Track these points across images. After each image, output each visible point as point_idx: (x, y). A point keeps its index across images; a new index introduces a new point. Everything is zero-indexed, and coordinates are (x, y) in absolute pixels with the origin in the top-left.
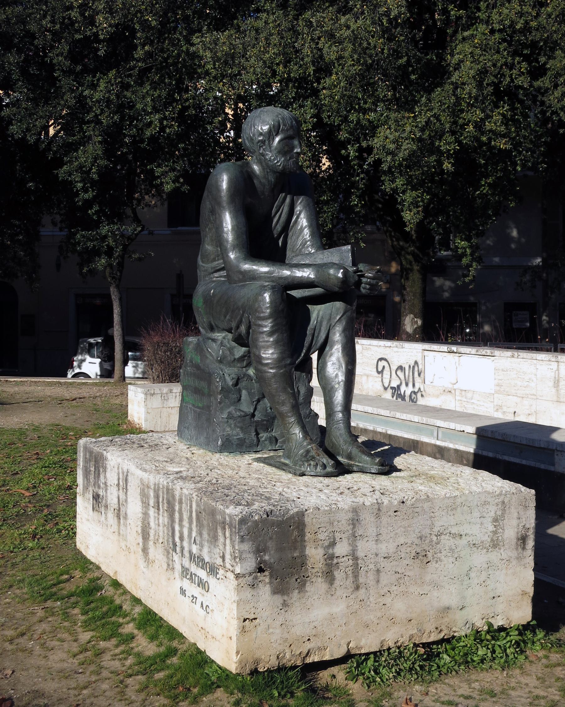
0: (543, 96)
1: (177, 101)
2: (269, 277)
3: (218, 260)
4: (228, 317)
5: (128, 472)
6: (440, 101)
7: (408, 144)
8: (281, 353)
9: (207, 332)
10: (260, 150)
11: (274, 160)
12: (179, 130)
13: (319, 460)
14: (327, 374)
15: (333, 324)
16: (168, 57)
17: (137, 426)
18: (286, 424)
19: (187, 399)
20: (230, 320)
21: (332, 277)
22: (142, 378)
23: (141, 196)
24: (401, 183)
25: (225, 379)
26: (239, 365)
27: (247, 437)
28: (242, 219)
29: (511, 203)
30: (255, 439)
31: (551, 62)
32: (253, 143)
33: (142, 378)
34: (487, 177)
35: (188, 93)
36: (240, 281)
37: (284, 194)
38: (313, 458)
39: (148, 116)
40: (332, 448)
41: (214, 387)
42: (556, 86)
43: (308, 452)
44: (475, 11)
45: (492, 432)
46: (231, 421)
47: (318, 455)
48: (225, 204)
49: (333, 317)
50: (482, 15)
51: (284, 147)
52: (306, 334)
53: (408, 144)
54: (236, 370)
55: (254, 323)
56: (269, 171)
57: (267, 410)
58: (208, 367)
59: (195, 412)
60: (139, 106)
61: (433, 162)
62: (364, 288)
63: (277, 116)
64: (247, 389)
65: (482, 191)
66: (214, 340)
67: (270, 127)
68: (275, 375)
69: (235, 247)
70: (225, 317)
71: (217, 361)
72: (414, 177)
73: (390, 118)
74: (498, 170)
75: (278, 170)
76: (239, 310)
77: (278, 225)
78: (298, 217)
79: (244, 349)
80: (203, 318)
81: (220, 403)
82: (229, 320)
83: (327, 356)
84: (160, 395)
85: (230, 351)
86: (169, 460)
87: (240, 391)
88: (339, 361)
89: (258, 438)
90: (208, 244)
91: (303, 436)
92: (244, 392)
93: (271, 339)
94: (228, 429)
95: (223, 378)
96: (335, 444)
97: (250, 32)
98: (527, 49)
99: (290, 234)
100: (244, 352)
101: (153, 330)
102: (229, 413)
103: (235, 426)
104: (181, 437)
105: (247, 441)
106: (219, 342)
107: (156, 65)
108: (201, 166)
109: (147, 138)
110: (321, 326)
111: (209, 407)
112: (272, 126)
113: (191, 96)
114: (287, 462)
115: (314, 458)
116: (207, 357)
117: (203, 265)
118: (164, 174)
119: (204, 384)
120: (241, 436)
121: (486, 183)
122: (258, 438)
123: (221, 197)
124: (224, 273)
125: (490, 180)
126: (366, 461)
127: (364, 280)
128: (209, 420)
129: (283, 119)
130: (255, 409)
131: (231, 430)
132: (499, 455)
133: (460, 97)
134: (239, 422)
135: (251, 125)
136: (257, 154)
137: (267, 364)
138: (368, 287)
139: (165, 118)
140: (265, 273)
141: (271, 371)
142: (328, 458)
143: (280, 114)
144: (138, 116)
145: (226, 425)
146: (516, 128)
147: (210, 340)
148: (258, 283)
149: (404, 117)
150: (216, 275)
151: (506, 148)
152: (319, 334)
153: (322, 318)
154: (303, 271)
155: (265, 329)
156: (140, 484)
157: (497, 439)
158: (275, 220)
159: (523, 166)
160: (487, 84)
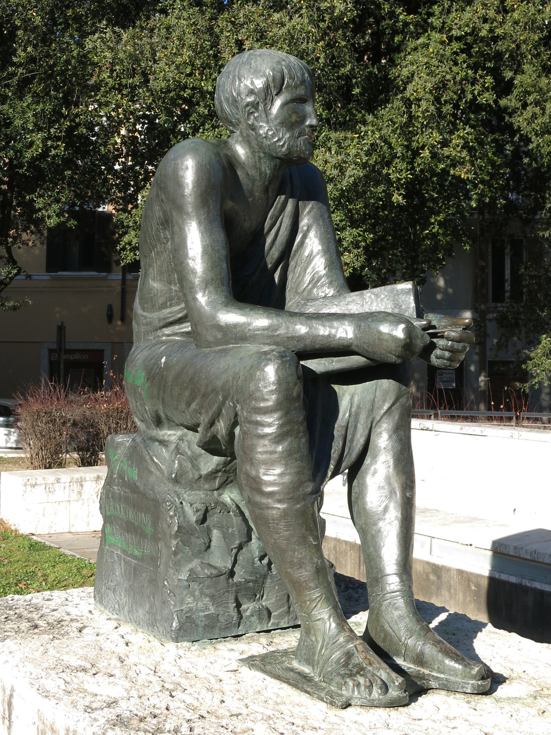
0: (511, 117)
1: (65, 117)
2: (269, 337)
3: (171, 306)
4: (193, 406)
5: (12, 690)
6: (391, 120)
7: (353, 169)
8: (299, 473)
9: (148, 428)
10: (248, 119)
11: (273, 136)
12: (65, 155)
13: (374, 675)
14: (364, 503)
15: (378, 418)
16: (55, 65)
17: (13, 528)
18: (305, 602)
19: (111, 539)
20: (198, 412)
21: (386, 337)
22: (16, 448)
23: (18, 234)
24: (338, 218)
25: (184, 512)
26: (207, 486)
27: (222, 612)
28: (220, 236)
29: (465, 245)
30: (235, 614)
31: (519, 77)
32: (237, 108)
33: (16, 448)
34: (438, 214)
35: (78, 108)
36: (218, 343)
37: (283, 197)
38: (361, 670)
39: (28, 134)
40: (384, 640)
41: (165, 526)
42: (525, 106)
43: (349, 655)
44: (426, 17)
45: (516, 548)
46: (194, 586)
47: (370, 664)
48: (190, 209)
49: (376, 405)
50: (435, 21)
51: (290, 116)
52: (333, 437)
53: (353, 169)
54: (201, 494)
55: (246, 418)
56: (262, 155)
57: (253, 563)
58: (152, 490)
59: (126, 563)
60: (18, 122)
61: (381, 193)
62: (437, 357)
63: (279, 63)
64: (220, 528)
65: (431, 230)
66: (163, 443)
67: (267, 80)
68: (285, 514)
69: (206, 284)
70: (189, 405)
71: (170, 479)
72: (354, 212)
73: (330, 138)
74: (450, 206)
75: (280, 155)
76: (217, 395)
77: (273, 249)
78: (305, 237)
79: (216, 459)
80: (143, 405)
81: (175, 553)
82: (195, 411)
83: (367, 473)
84: (44, 486)
85: (192, 462)
86: (88, 666)
87: (208, 532)
88: (390, 484)
89: (239, 612)
90: (153, 280)
91: (338, 624)
92: (216, 533)
93: (280, 448)
94: (190, 600)
95: (180, 511)
96: (391, 635)
97: (159, 30)
98: (490, 62)
99: (292, 264)
100: (218, 465)
101: (32, 396)
102: (191, 570)
103: (202, 593)
104: (101, 602)
105: (222, 619)
106: (173, 447)
107: (40, 74)
108: (89, 199)
109: (27, 162)
110: (356, 421)
111: (154, 560)
112: (270, 79)
113: (82, 111)
114: (306, 669)
115: (363, 669)
116: (151, 472)
117: (145, 314)
118: (47, 207)
119: (145, 519)
120: (212, 610)
121: (436, 220)
122: (239, 612)
123: (183, 196)
124: (187, 327)
125: (441, 217)
126: (455, 670)
127: (440, 342)
128: (153, 581)
129: (289, 67)
130: (235, 562)
131: (194, 600)
132: (527, 581)
133: (414, 115)
134: (208, 587)
135: (234, 77)
136: (243, 126)
137: (271, 494)
138: (447, 354)
139: (49, 138)
140: (264, 329)
141: (279, 506)
142: (389, 670)
143: (284, 60)
144: (16, 135)
145: (185, 593)
146: (471, 156)
147: (157, 443)
148: (252, 348)
149: (346, 138)
150: (167, 331)
151: (468, 178)
152: (354, 435)
153: (359, 407)
154: (331, 327)
155: (268, 430)
156: (36, 720)
157: (525, 559)
158: (269, 240)
159: (479, 201)
160: (446, 102)
